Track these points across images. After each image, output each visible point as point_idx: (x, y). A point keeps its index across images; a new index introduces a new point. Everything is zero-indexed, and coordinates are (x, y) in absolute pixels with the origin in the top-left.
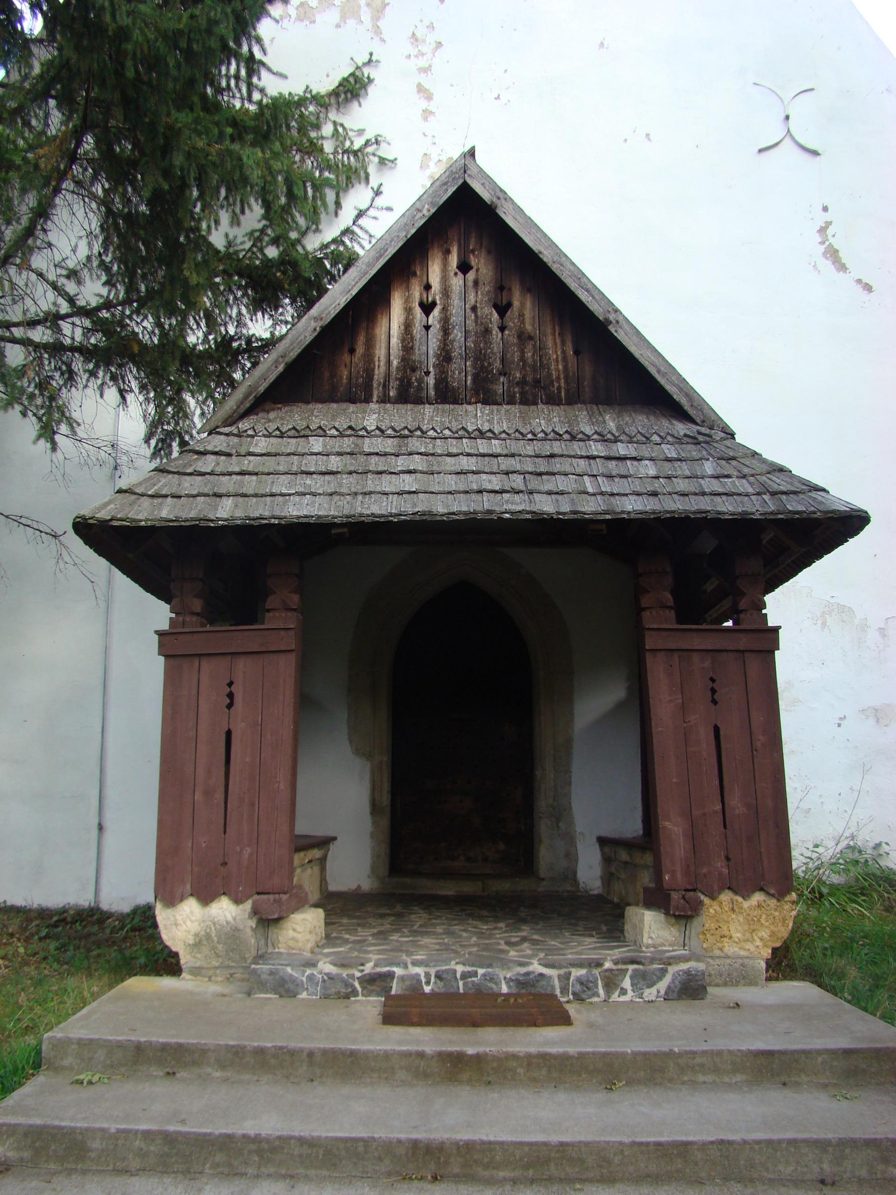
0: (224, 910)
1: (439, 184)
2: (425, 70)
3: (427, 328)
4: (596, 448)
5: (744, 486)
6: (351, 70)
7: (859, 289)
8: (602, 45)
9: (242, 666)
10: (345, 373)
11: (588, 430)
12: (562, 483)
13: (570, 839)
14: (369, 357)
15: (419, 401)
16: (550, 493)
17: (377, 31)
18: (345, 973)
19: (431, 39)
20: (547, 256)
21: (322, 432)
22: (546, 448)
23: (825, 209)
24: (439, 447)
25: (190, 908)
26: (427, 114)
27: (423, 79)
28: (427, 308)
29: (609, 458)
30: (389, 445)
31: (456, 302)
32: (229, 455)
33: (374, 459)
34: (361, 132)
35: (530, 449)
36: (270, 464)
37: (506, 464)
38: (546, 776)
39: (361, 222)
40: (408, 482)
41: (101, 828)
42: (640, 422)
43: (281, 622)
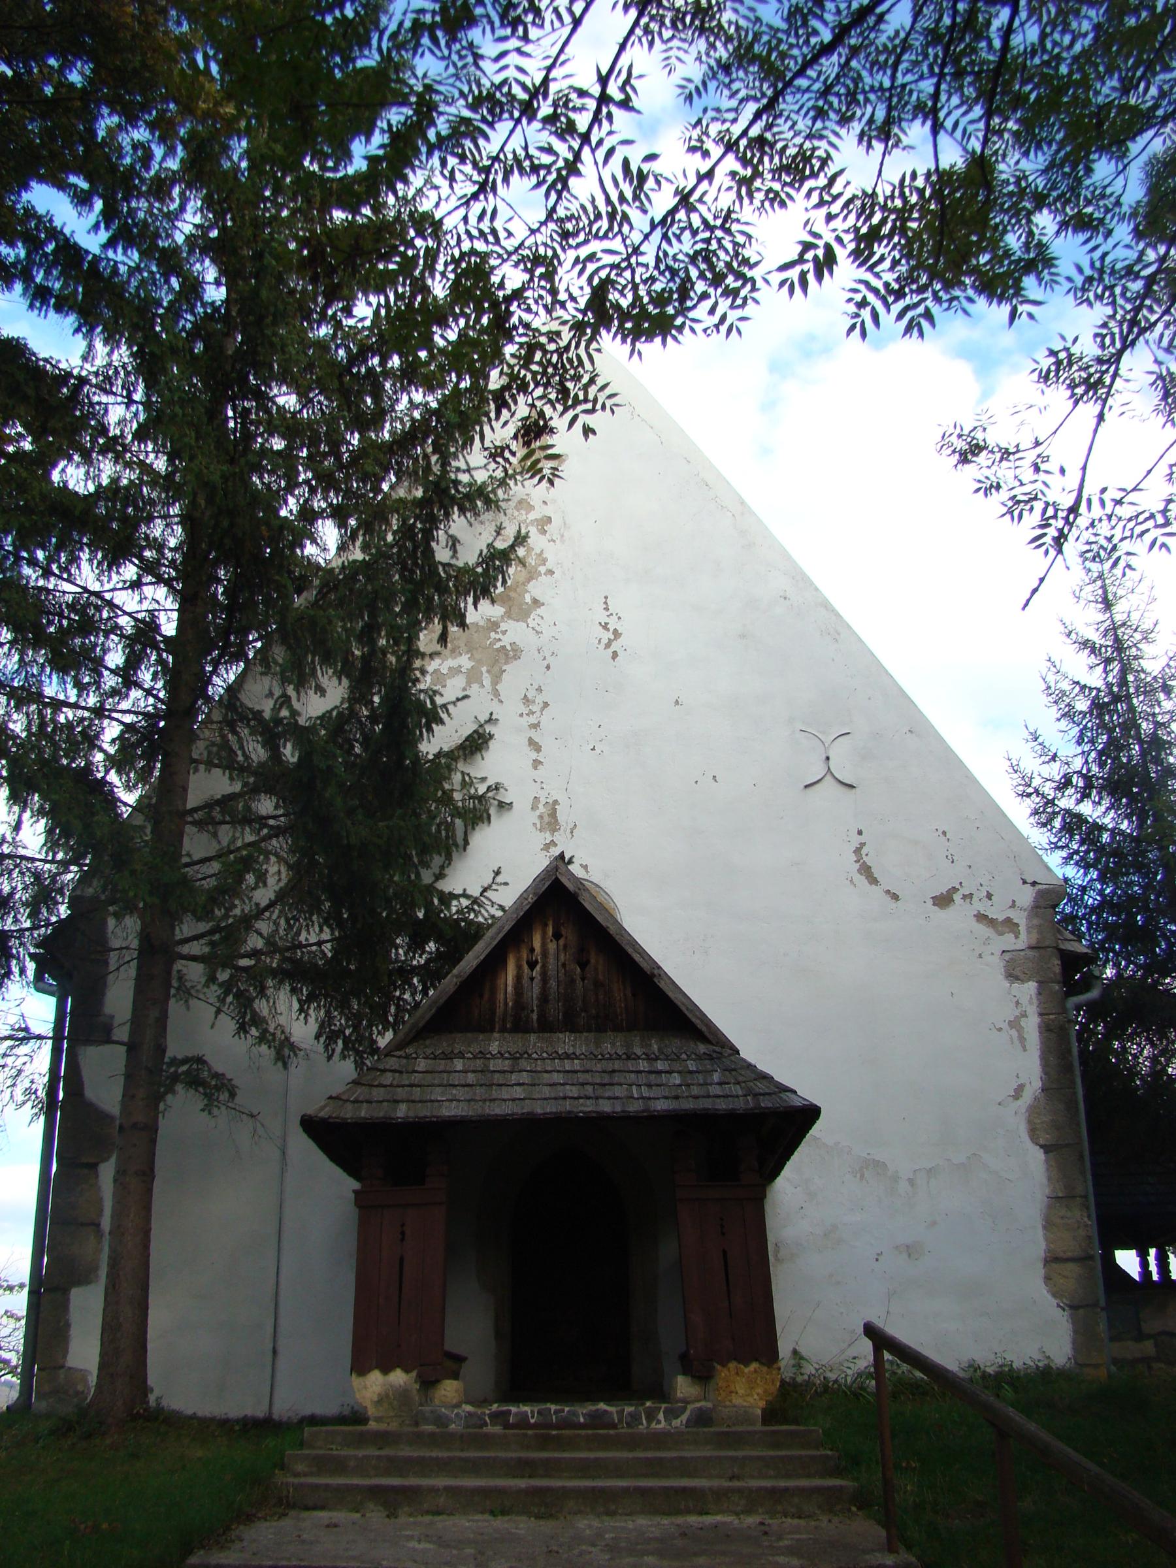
0: (398, 1377)
1: (539, 879)
2: (535, 726)
3: (532, 979)
4: (643, 1065)
5: (737, 1090)
8: (677, 702)
12: (618, 1091)
16: (609, 1098)
17: (496, 693)
19: (539, 700)
21: (461, 1055)
22: (610, 1066)
23: (860, 833)
26: (536, 764)
27: (533, 734)
28: (532, 965)
29: (650, 1072)
31: (551, 960)
32: (401, 1072)
33: (497, 1076)
34: (484, 779)
37: (582, 1077)
40: (519, 1092)
41: (275, 1352)
42: (675, 1044)
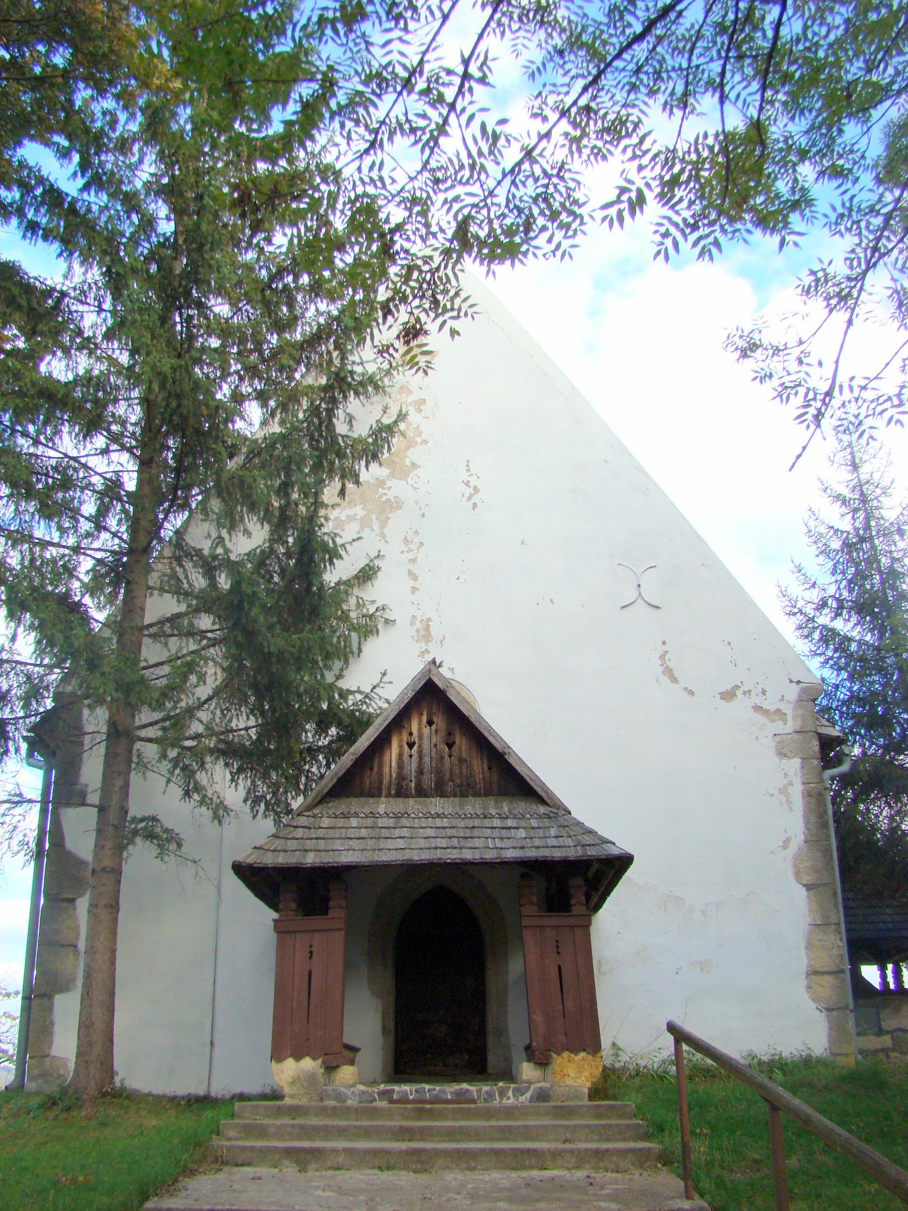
0: (308, 1064)
2: (413, 561)
4: (497, 823)
5: (569, 842)
6: (367, 561)
7: (685, 693)
8: (523, 542)
9: (317, 937)
10: (368, 782)
11: (493, 812)
12: (477, 843)
13: (507, 1048)
14: (380, 773)
15: (407, 796)
16: (470, 848)
17: (383, 535)
18: (370, 1090)
19: (417, 540)
20: (473, 718)
21: (356, 815)
22: (471, 823)
23: (664, 643)
24: (417, 823)
25: (290, 1062)
26: (414, 590)
27: (411, 566)
28: (411, 745)
30: (391, 822)
31: (426, 742)
33: (383, 830)
34: (373, 602)
35: (462, 824)
36: (331, 833)
37: (450, 832)
38: (492, 1010)
39: (377, 690)
40: (401, 843)
41: (212, 1044)
42: (521, 806)
43: (337, 914)
